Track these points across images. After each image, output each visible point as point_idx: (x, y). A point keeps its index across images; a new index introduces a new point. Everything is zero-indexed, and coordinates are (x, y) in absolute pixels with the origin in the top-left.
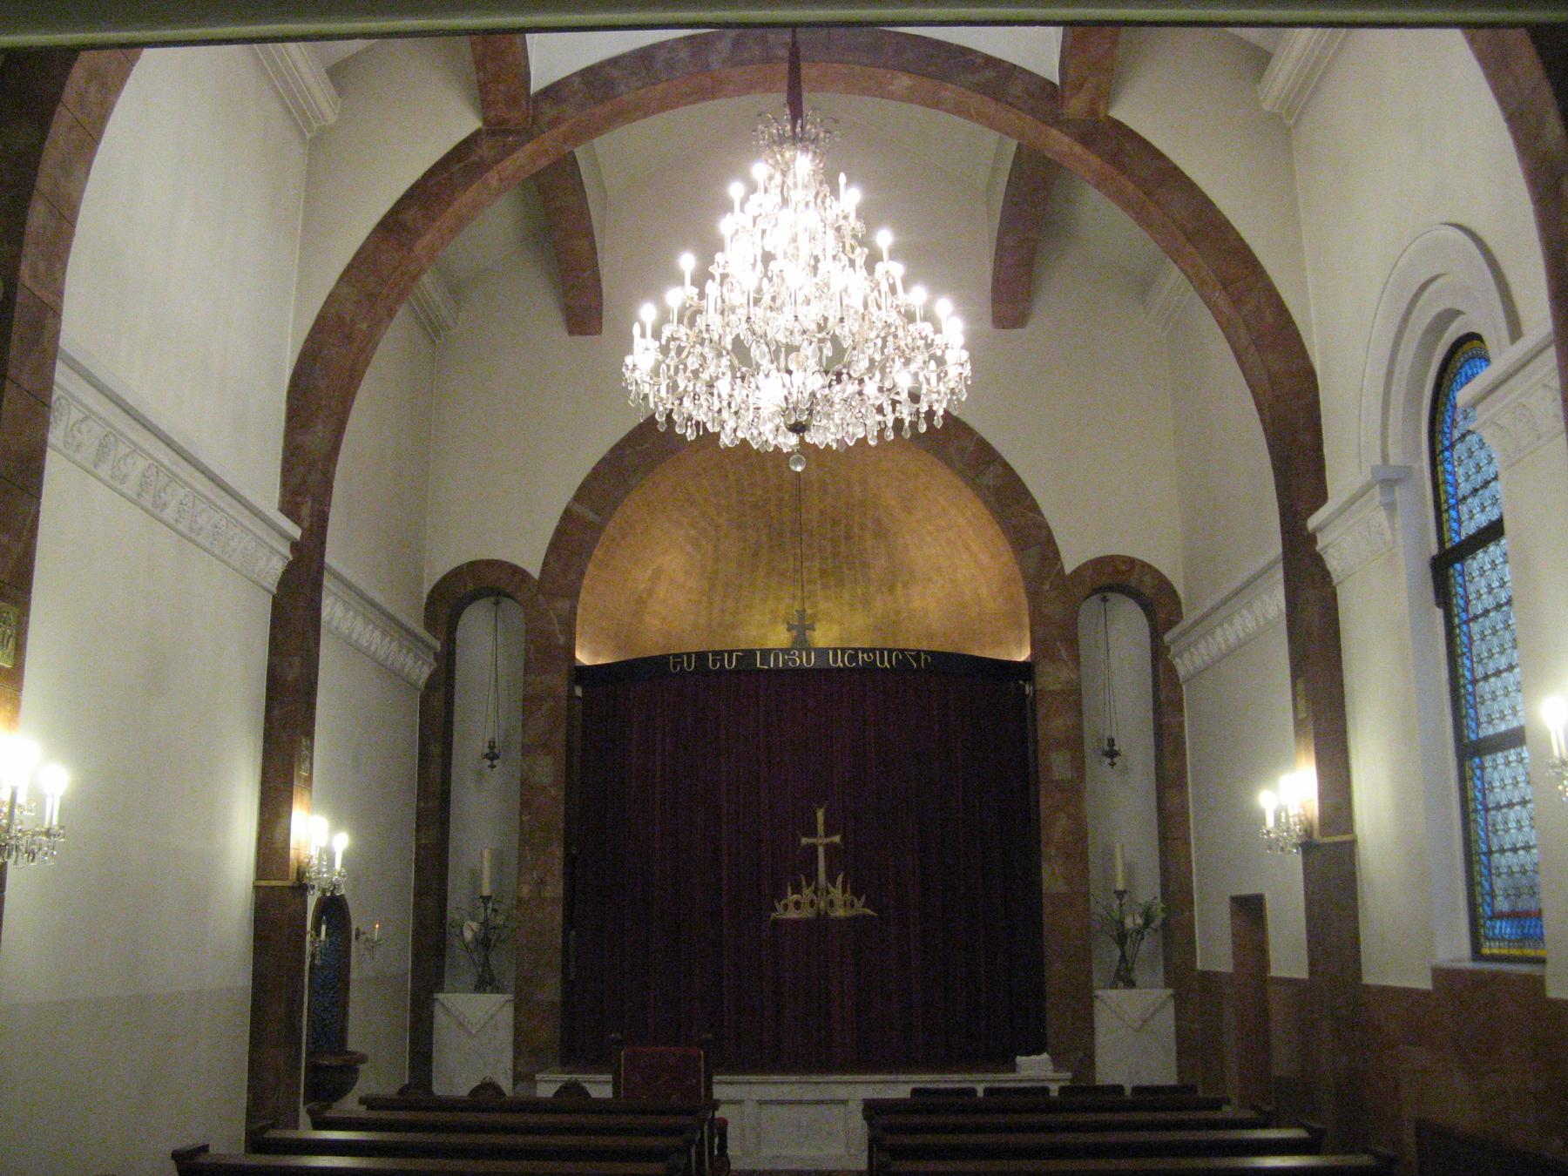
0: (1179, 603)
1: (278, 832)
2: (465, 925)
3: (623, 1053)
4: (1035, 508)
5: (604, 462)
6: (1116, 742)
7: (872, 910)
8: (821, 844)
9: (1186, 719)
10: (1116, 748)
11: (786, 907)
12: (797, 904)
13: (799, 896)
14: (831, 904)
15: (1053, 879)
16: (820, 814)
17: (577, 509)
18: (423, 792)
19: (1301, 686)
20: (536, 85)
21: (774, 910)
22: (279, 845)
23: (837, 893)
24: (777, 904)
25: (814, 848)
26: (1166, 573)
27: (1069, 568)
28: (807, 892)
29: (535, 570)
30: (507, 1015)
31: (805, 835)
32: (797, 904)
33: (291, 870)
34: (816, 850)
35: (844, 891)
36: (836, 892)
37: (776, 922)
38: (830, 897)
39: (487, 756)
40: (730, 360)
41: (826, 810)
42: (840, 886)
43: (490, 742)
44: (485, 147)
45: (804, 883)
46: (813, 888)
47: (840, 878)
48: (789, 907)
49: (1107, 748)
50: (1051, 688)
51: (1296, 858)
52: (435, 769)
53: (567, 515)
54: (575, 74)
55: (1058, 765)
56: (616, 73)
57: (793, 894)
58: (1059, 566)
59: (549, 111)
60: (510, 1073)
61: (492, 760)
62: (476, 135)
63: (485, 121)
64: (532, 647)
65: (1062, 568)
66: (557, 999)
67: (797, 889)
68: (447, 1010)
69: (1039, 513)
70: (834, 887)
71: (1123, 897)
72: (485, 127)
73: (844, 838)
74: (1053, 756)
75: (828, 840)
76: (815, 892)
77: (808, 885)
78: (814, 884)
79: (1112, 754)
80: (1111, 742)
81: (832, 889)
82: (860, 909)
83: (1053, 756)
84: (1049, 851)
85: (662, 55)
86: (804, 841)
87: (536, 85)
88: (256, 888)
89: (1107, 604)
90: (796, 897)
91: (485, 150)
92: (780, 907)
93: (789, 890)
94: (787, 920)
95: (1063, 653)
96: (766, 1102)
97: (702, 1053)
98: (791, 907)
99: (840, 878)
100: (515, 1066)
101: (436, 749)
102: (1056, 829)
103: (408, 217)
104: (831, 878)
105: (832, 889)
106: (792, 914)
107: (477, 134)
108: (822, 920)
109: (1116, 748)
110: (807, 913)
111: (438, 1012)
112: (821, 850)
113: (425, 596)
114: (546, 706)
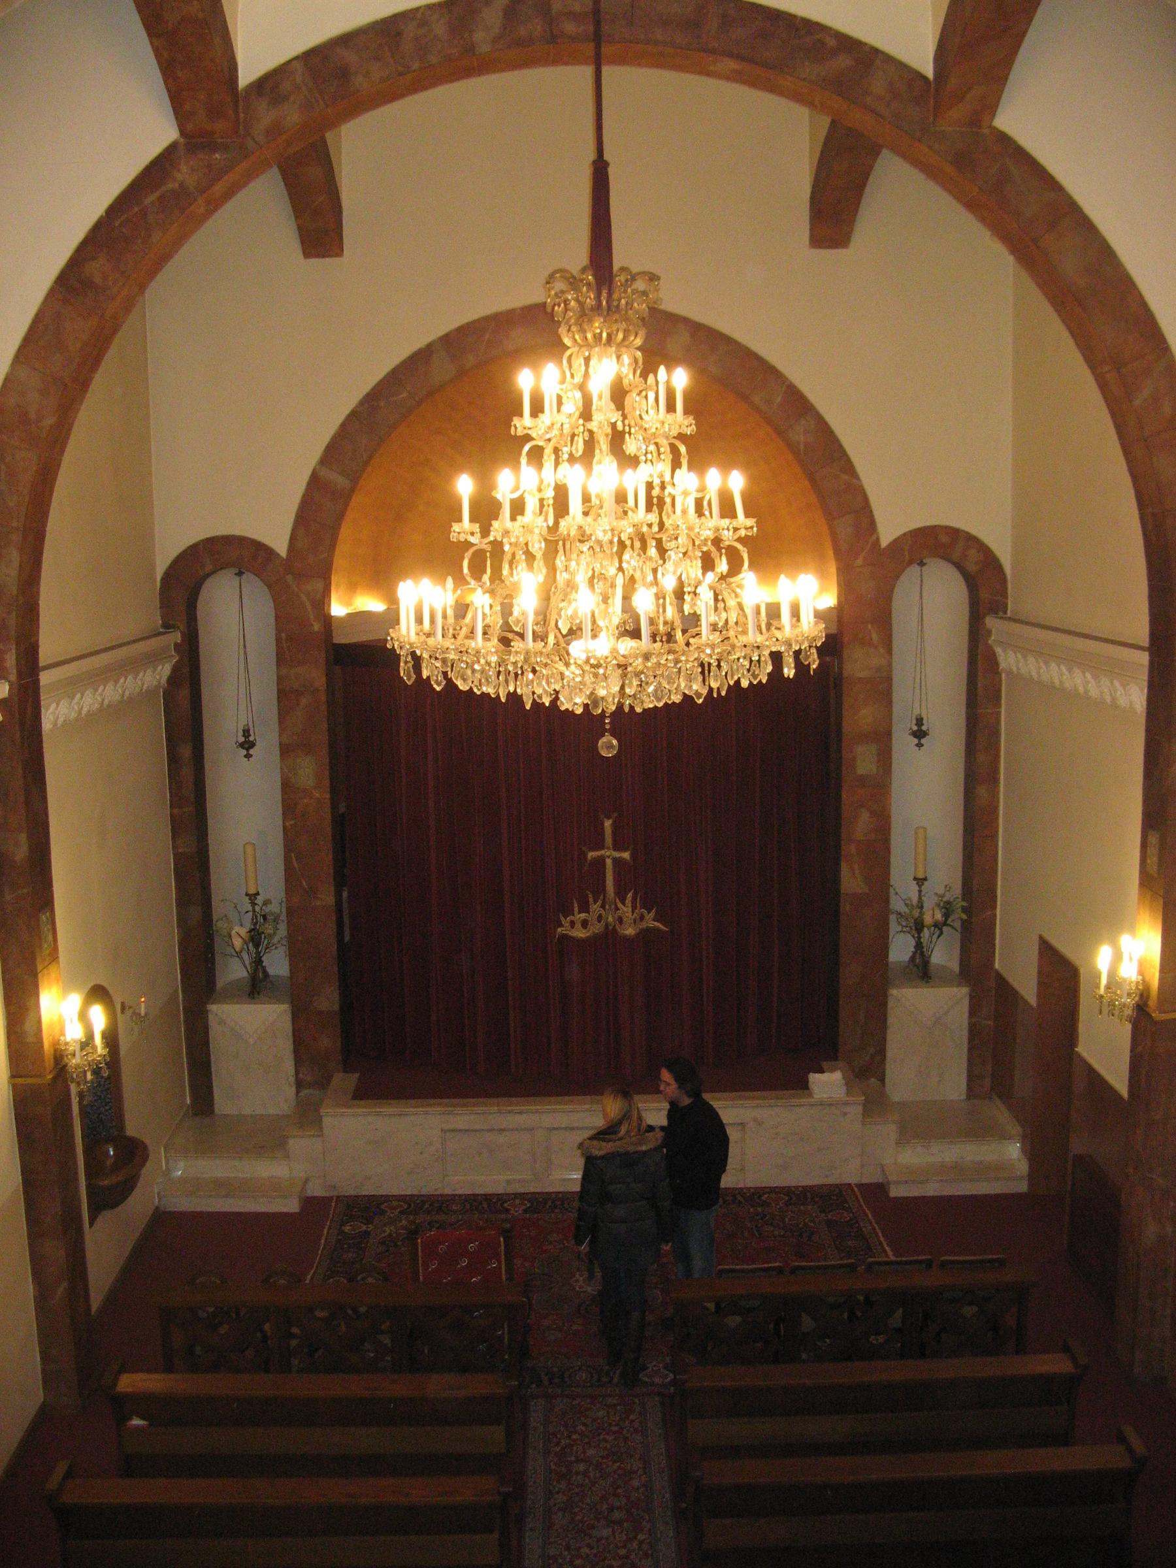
0: (1004, 580)
1: (28, 1026)
2: (234, 932)
3: (419, 1241)
4: (849, 468)
5: (353, 415)
6: (925, 722)
7: (663, 925)
8: (608, 849)
9: (1003, 710)
10: (924, 728)
11: (573, 924)
12: (585, 924)
13: (586, 914)
14: (620, 920)
15: (851, 880)
16: (608, 824)
17: (325, 473)
18: (176, 799)
19: (1153, 839)
20: (246, 75)
21: (561, 925)
22: (30, 1039)
23: (626, 910)
24: (562, 919)
25: (601, 861)
26: (993, 546)
27: (885, 542)
28: (595, 907)
29: (280, 545)
30: (286, 1023)
31: (592, 849)
32: (585, 924)
33: (46, 1058)
34: (604, 861)
35: (634, 908)
36: (625, 909)
37: (565, 937)
38: (619, 913)
39: (242, 745)
40: (512, 574)
41: (615, 822)
42: (630, 905)
43: (244, 731)
44: (184, 169)
45: (591, 900)
46: (599, 903)
47: (630, 895)
48: (576, 926)
49: (915, 728)
50: (861, 675)
51: (1124, 1033)
52: (187, 772)
53: (315, 481)
54: (297, 58)
55: (863, 761)
56: (351, 57)
57: (580, 912)
58: (874, 537)
59: (265, 115)
60: (292, 1080)
61: (248, 750)
62: (169, 153)
63: (182, 133)
64: (283, 635)
65: (878, 539)
66: (336, 1007)
67: (584, 908)
68: (222, 1022)
69: (857, 477)
70: (624, 904)
71: (923, 884)
72: (182, 140)
73: (633, 856)
74: (860, 749)
75: (617, 854)
76: (603, 906)
77: (595, 901)
78: (602, 897)
79: (920, 734)
80: (920, 721)
81: (620, 905)
82: (650, 922)
83: (860, 749)
84: (849, 849)
85: (410, 30)
86: (591, 855)
87: (246, 75)
88: (15, 1087)
89: (924, 568)
90: (583, 916)
91: (185, 174)
92: (565, 922)
93: (576, 909)
94: (573, 938)
95: (875, 637)
96: (554, 1129)
97: (502, 1239)
98: (578, 925)
99: (630, 895)
100: (297, 1073)
101: (186, 751)
102: (860, 825)
103: (96, 268)
104: (621, 895)
105: (620, 905)
106: (579, 933)
107: (171, 149)
108: (610, 936)
109: (924, 728)
110: (596, 928)
111: (212, 1021)
112: (609, 862)
113: (158, 584)
114: (304, 701)
